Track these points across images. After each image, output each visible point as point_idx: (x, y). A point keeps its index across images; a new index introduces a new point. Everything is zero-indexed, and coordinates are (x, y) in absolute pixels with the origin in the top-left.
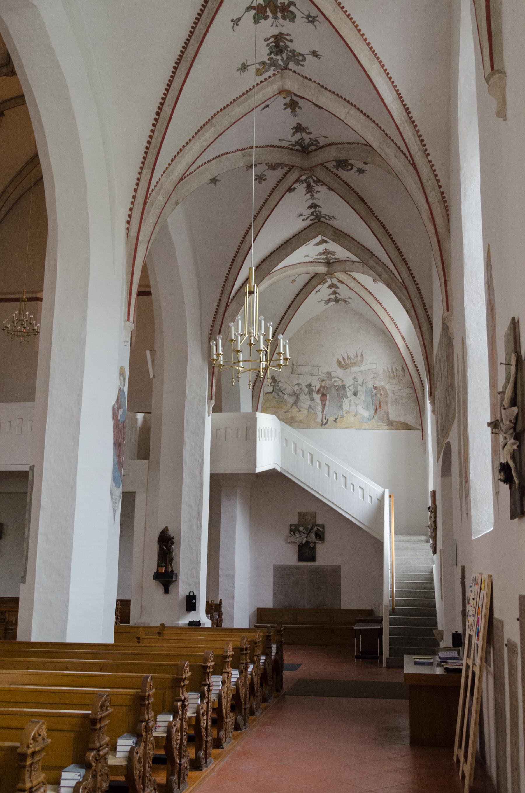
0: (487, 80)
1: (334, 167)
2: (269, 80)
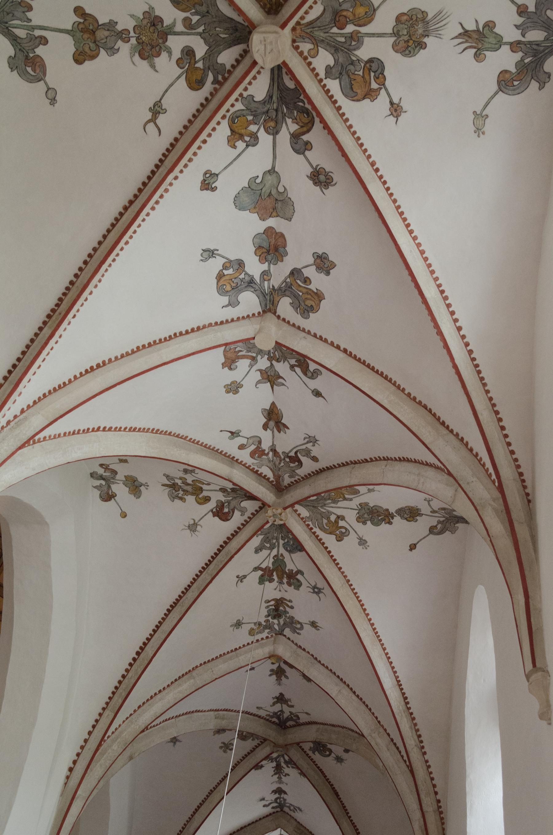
0: (528, 677)
1: (310, 749)
2: (261, 642)
